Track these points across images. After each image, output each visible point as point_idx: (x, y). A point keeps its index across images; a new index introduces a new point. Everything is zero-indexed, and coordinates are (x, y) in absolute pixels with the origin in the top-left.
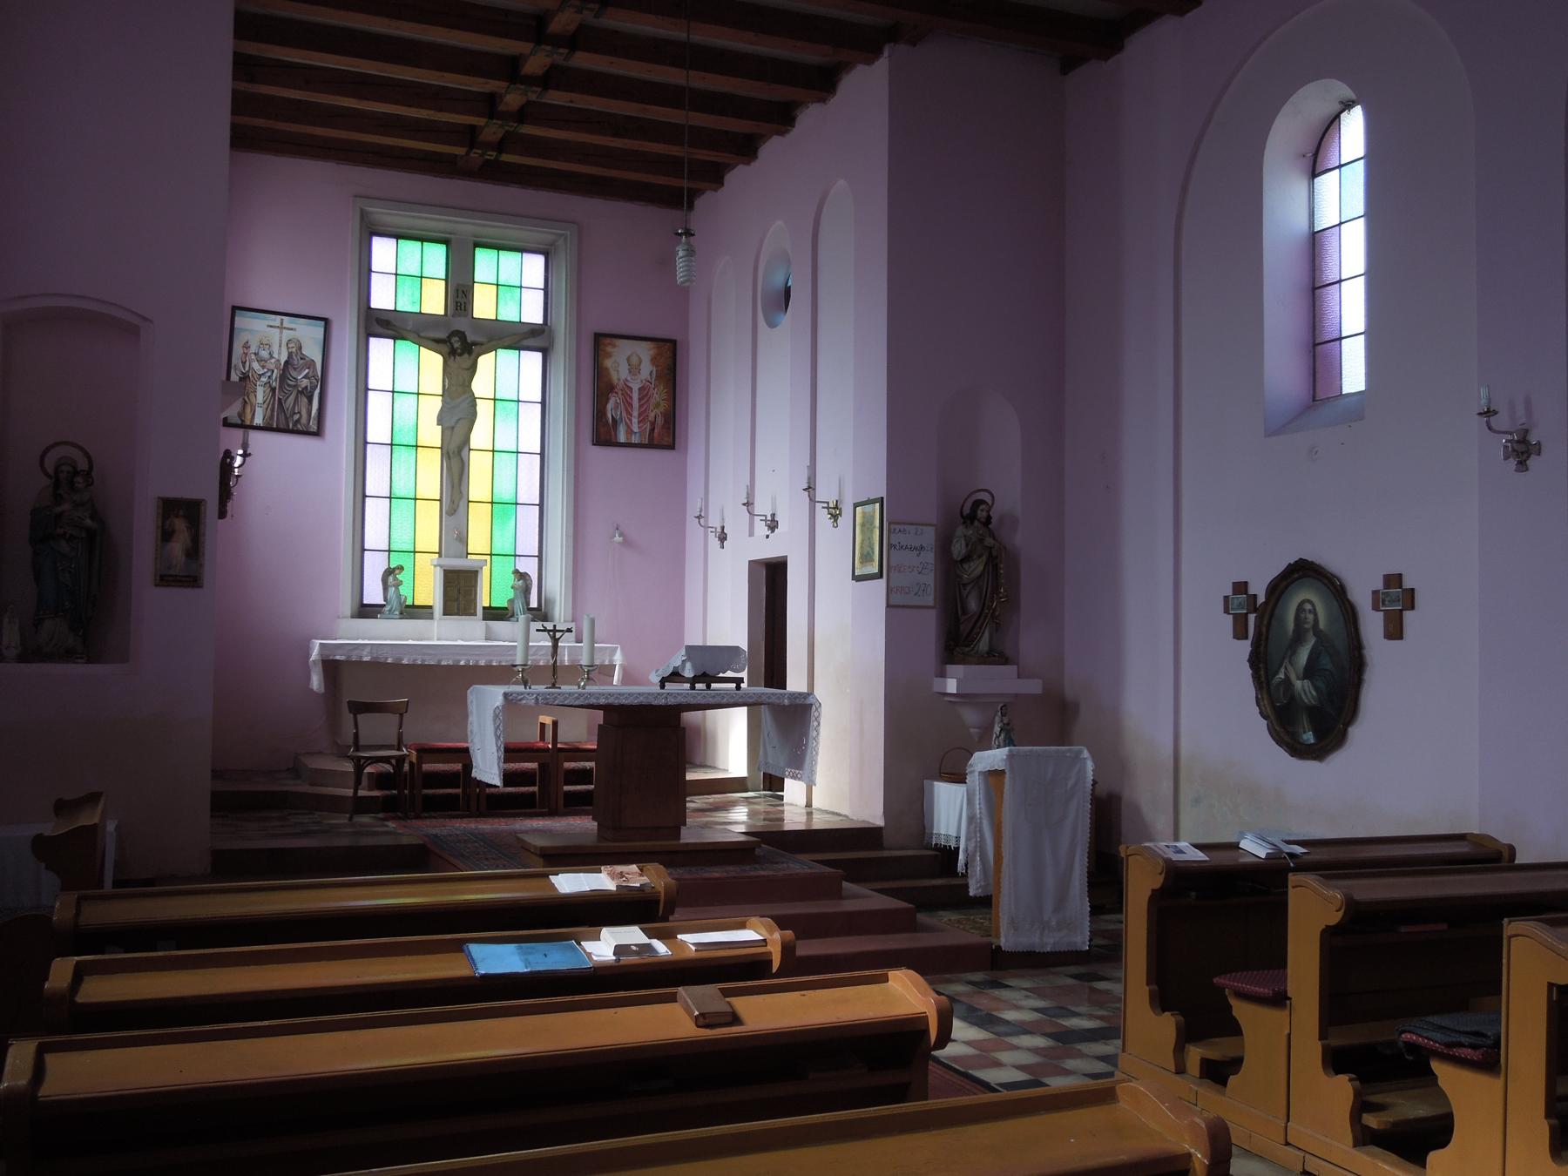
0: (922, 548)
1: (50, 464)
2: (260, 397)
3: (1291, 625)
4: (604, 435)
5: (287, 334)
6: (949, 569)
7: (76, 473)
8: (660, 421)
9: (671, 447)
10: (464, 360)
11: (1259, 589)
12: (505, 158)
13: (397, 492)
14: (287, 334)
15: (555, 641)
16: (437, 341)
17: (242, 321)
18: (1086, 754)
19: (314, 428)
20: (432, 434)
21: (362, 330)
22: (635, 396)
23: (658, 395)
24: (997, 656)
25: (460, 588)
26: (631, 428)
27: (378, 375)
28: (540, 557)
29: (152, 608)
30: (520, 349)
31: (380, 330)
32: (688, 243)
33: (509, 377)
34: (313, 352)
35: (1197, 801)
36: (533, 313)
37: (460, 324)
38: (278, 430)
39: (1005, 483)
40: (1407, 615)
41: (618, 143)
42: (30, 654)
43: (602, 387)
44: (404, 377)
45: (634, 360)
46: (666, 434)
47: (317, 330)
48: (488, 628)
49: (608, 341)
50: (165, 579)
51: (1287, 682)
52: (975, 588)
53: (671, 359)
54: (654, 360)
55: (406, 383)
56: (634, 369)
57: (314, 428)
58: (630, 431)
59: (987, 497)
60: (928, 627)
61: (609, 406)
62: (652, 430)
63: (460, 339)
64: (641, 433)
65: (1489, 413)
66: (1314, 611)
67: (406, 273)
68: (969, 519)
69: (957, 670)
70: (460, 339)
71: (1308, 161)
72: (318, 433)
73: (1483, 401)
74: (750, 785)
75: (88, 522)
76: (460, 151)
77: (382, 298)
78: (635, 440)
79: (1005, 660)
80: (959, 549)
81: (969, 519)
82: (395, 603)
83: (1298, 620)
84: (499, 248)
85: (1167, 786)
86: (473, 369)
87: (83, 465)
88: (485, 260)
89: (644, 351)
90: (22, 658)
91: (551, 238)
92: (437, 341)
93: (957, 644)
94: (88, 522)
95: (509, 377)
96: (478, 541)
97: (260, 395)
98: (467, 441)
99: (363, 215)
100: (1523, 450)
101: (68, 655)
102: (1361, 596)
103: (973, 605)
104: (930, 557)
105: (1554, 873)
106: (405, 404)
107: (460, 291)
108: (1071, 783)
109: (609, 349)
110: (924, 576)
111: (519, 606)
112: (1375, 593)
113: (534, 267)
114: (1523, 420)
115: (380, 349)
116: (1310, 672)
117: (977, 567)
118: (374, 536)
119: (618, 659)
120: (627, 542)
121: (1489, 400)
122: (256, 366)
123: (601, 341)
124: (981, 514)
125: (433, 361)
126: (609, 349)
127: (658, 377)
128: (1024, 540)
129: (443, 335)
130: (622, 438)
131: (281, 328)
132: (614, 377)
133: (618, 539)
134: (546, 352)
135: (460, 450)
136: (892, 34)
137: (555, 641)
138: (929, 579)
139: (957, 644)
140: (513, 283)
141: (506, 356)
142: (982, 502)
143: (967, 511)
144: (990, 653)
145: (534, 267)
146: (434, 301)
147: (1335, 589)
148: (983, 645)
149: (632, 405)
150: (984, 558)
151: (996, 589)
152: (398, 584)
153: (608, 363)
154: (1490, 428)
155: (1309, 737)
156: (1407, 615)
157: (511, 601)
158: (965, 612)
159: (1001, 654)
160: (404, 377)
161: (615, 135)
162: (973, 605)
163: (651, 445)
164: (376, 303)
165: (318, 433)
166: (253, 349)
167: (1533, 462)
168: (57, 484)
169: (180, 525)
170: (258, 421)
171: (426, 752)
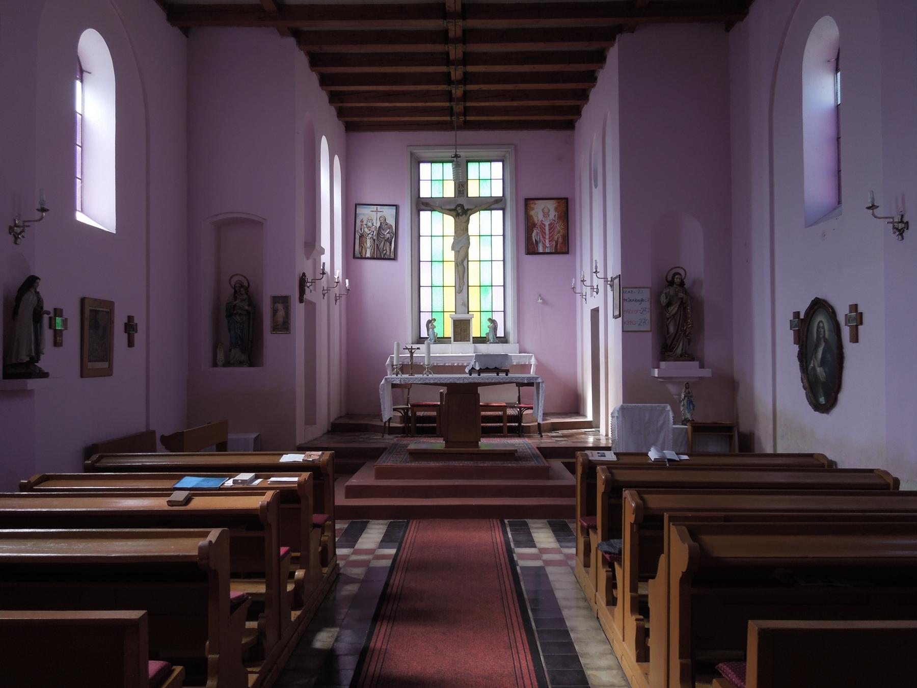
0: (642, 300)
2: (369, 245)
4: (531, 250)
5: (379, 214)
6: (661, 311)
7: (242, 286)
8: (560, 240)
9: (567, 253)
10: (464, 218)
12: (468, 118)
13: (434, 284)
14: (379, 214)
15: (412, 353)
16: (450, 210)
17: (360, 210)
18: (669, 408)
19: (392, 256)
20: (450, 255)
21: (414, 207)
22: (547, 228)
23: (559, 227)
24: (688, 356)
25: (461, 328)
26: (546, 244)
27: (424, 229)
28: (504, 311)
29: (271, 341)
30: (491, 210)
31: (423, 207)
32: (457, 162)
34: (391, 221)
36: (498, 192)
37: (461, 201)
39: (694, 263)
40: (860, 327)
41: (515, 104)
42: (228, 363)
43: (530, 225)
44: (437, 227)
45: (546, 210)
46: (564, 246)
47: (392, 211)
50: (276, 328)
51: (814, 368)
52: (674, 318)
53: (566, 209)
54: (556, 209)
55: (437, 231)
56: (546, 215)
57: (392, 256)
58: (544, 246)
60: (648, 343)
61: (534, 234)
62: (556, 245)
63: (461, 208)
65: (872, 207)
66: (823, 328)
67: (436, 179)
68: (671, 283)
69: (663, 364)
70: (461, 208)
71: (833, 64)
73: (869, 200)
74: (594, 425)
75: (247, 308)
76: (448, 118)
77: (425, 193)
78: (547, 250)
80: (663, 300)
81: (671, 283)
82: (432, 336)
84: (479, 161)
85: (771, 426)
86: (468, 221)
87: (246, 284)
88: (472, 168)
89: (551, 205)
90: (224, 366)
91: (503, 153)
92: (450, 210)
93: (666, 350)
94: (247, 308)
95: (488, 226)
96: (473, 306)
97: (369, 243)
99: (412, 154)
100: (901, 228)
101: (241, 364)
103: (672, 329)
104: (647, 305)
105: (842, 474)
106: (437, 242)
107: (461, 186)
108: (660, 423)
109: (532, 206)
110: (645, 316)
111: (491, 337)
112: (846, 315)
113: (498, 167)
115: (425, 216)
116: (823, 363)
118: (425, 305)
119: (533, 361)
120: (545, 302)
121: (873, 199)
122: (366, 230)
123: (528, 202)
124: (677, 280)
125: (450, 220)
126: (532, 206)
127: (559, 218)
128: (706, 293)
129: (453, 207)
131: (377, 211)
132: (536, 219)
133: (540, 301)
134: (504, 210)
135: (463, 262)
136: (620, 29)
137: (412, 353)
138: (647, 316)
139: (666, 350)
140: (487, 178)
141: (485, 214)
142: (678, 274)
143: (670, 278)
144: (681, 355)
145: (498, 167)
146: (449, 191)
147: (832, 313)
148: (679, 351)
149: (543, 234)
150: (678, 304)
151: (685, 320)
153: (532, 213)
154: (875, 217)
155: (822, 400)
156: (860, 327)
157: (487, 334)
158: (668, 333)
160: (437, 227)
161: (512, 100)
162: (672, 329)
163: (556, 252)
167: (906, 234)
168: (235, 292)
169: (280, 306)
170: (368, 255)
171: (416, 406)
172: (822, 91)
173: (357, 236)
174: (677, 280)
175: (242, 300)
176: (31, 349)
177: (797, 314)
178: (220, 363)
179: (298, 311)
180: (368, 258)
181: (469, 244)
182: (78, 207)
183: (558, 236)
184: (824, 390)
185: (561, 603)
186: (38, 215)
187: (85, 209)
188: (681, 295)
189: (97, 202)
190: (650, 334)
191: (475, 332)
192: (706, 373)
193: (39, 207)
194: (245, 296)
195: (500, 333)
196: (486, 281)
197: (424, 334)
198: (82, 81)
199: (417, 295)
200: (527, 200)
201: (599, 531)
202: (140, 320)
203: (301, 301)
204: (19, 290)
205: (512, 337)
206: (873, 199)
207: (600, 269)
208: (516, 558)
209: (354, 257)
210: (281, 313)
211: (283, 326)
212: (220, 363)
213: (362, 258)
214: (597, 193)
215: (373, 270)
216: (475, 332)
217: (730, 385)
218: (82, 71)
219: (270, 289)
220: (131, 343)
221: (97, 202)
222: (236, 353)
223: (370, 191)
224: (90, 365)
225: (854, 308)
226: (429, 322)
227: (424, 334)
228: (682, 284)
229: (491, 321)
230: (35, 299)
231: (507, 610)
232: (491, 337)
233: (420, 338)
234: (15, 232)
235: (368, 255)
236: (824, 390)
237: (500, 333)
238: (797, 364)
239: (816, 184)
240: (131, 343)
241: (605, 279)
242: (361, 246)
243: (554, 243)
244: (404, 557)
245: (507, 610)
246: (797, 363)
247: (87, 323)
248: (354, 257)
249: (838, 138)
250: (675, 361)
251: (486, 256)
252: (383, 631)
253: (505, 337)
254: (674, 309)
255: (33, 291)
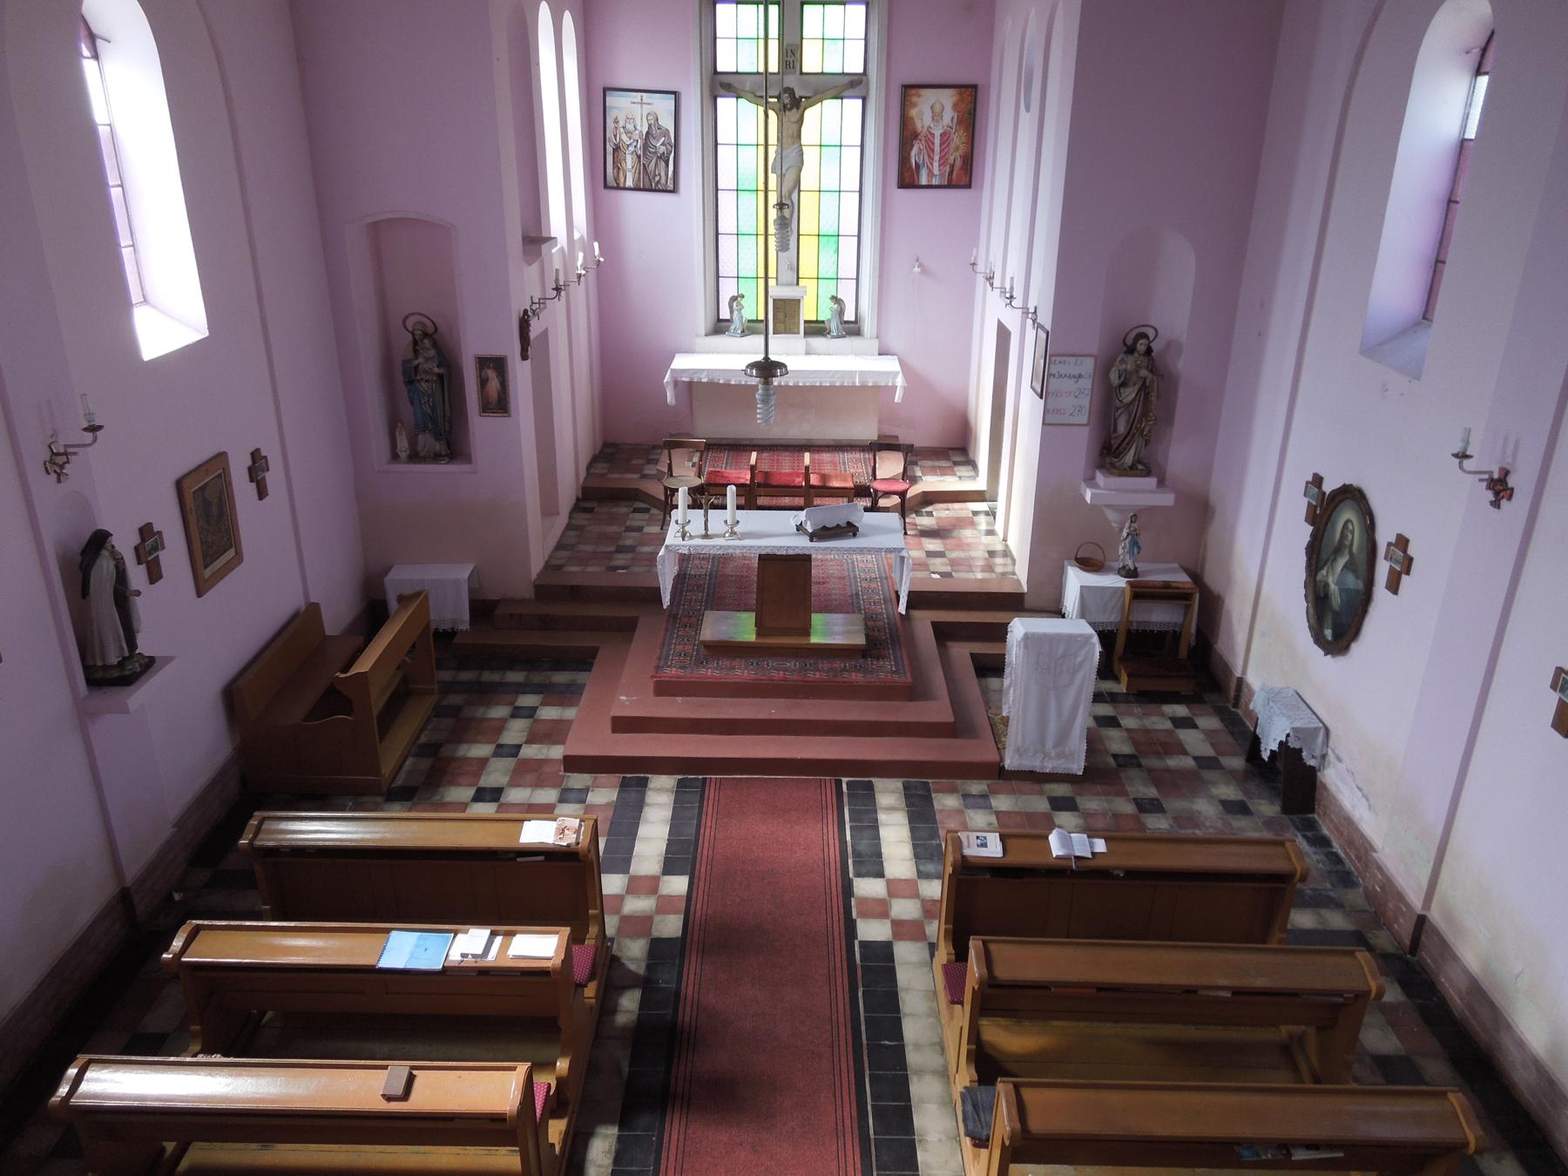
1: (409, 324)
3: (1338, 536)
4: (908, 180)
7: (426, 335)
8: (958, 163)
9: (969, 186)
10: (792, 115)
11: (1328, 487)
13: (742, 230)
17: (614, 100)
19: (671, 186)
22: (937, 141)
23: (958, 140)
24: (1142, 468)
26: (932, 171)
29: (481, 428)
31: (722, 92)
33: (835, 127)
34: (667, 123)
35: (1264, 634)
37: (791, 81)
38: (644, 190)
39: (1173, 314)
42: (414, 457)
43: (908, 135)
45: (938, 108)
46: (963, 174)
47: (669, 102)
48: (808, 344)
49: (914, 91)
52: (1131, 405)
54: (955, 107)
56: (937, 116)
58: (931, 174)
59: (1151, 333)
60: (1081, 442)
61: (913, 153)
62: (951, 172)
63: (789, 93)
64: (942, 175)
65: (1462, 456)
68: (1131, 350)
70: (789, 93)
72: (674, 191)
75: (436, 370)
78: (935, 182)
79: (1148, 473)
80: (1114, 378)
83: (1343, 536)
87: (430, 329)
89: (947, 99)
93: (1110, 453)
94: (436, 370)
95: (835, 127)
97: (629, 162)
98: (798, 182)
101: (436, 458)
102: (1384, 536)
103: (1122, 427)
104: (1087, 383)
108: (1079, 659)
109: (914, 99)
110: (1080, 400)
114: (1509, 460)
115: (726, 105)
117: (1129, 394)
120: (925, 271)
122: (624, 137)
123: (909, 90)
124: (1141, 346)
126: (914, 99)
127: (960, 122)
128: (1185, 366)
130: (924, 181)
133: (917, 270)
135: (790, 193)
138: (1086, 402)
139: (1110, 453)
141: (831, 105)
143: (1129, 341)
144: (1132, 467)
148: (1129, 458)
150: (1137, 387)
151: (1145, 414)
152: (741, 308)
153: (913, 113)
155: (1328, 633)
158: (1115, 430)
159: (1147, 466)
162: (1122, 427)
163: (950, 185)
164: (722, 66)
165: (674, 191)
166: (621, 123)
168: (415, 343)
169: (491, 374)
170: (629, 183)
172: (1446, 105)
173: (610, 149)
174: (1141, 346)
175: (427, 360)
176: (122, 648)
177: (1318, 480)
178: (403, 455)
179: (521, 374)
180: (630, 189)
181: (802, 162)
182: (135, 295)
183: (955, 156)
184: (1337, 623)
185: (913, 1058)
186: (89, 436)
187: (150, 297)
188: (1144, 373)
189: (168, 307)
190: (1087, 429)
191: (808, 313)
192: (1167, 499)
193: (86, 425)
194: (432, 352)
195: (849, 315)
196: (828, 227)
197: (725, 314)
198: (96, 56)
199: (712, 218)
200: (907, 88)
201: (968, 1007)
202: (271, 452)
203: (524, 357)
204: (84, 552)
205: (868, 326)
206: (1467, 443)
207: (1018, 293)
208: (854, 915)
209: (606, 186)
210: (494, 385)
211: (499, 405)
212: (403, 455)
213: (618, 188)
214: (1028, 121)
215: (637, 208)
216: (808, 313)
217: (1200, 513)
218: (92, 38)
219: (473, 344)
220: (262, 493)
221: (168, 307)
222: (426, 441)
223: (632, 61)
224: (207, 573)
225: (1402, 542)
226: (734, 299)
227: (725, 314)
228: (1149, 351)
229: (835, 299)
230: (112, 564)
231: (841, 1154)
232: (833, 326)
233: (719, 320)
234: (57, 463)
235: (629, 183)
236: (1337, 623)
237: (849, 315)
238: (1302, 560)
239: (1394, 280)
240: (262, 493)
241: (1025, 311)
242: (617, 166)
243: (948, 168)
244: (698, 914)
245: (841, 1154)
246: (1308, 539)
247: (192, 519)
248: (606, 186)
249: (1451, 201)
250: (1120, 475)
251: (830, 183)
252: (676, 1124)
253: (856, 322)
254: (1129, 394)
255: (105, 553)
